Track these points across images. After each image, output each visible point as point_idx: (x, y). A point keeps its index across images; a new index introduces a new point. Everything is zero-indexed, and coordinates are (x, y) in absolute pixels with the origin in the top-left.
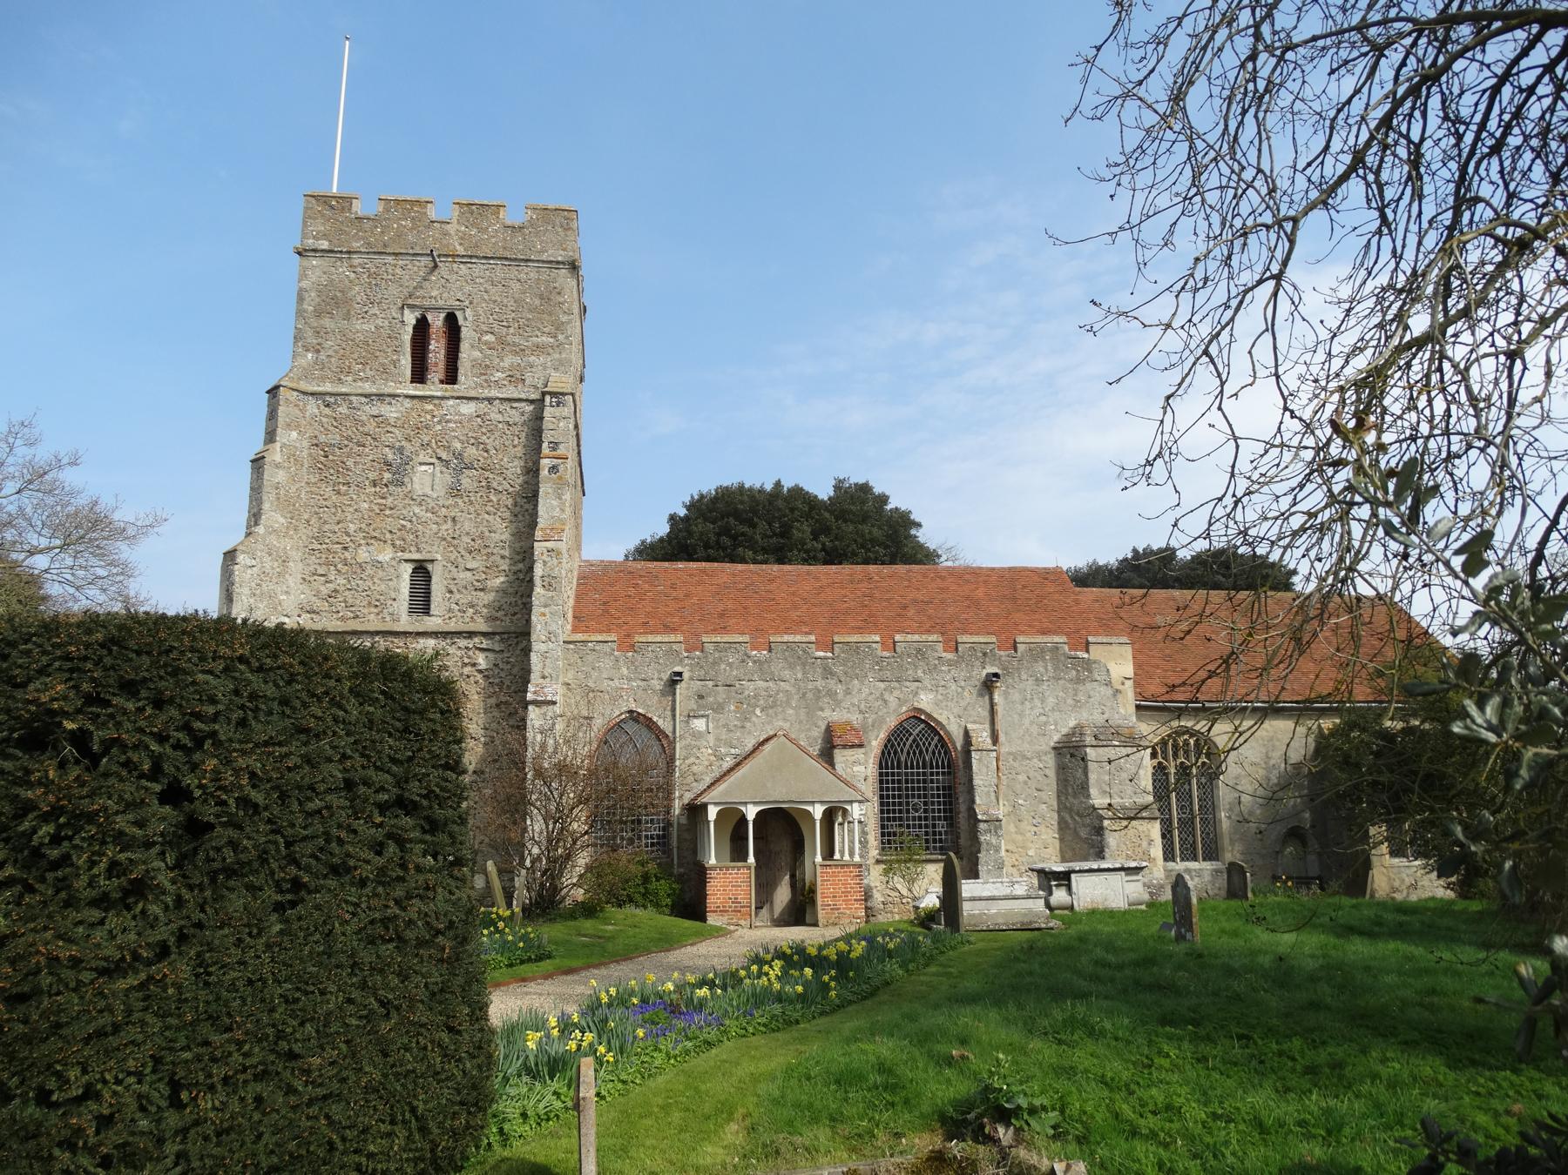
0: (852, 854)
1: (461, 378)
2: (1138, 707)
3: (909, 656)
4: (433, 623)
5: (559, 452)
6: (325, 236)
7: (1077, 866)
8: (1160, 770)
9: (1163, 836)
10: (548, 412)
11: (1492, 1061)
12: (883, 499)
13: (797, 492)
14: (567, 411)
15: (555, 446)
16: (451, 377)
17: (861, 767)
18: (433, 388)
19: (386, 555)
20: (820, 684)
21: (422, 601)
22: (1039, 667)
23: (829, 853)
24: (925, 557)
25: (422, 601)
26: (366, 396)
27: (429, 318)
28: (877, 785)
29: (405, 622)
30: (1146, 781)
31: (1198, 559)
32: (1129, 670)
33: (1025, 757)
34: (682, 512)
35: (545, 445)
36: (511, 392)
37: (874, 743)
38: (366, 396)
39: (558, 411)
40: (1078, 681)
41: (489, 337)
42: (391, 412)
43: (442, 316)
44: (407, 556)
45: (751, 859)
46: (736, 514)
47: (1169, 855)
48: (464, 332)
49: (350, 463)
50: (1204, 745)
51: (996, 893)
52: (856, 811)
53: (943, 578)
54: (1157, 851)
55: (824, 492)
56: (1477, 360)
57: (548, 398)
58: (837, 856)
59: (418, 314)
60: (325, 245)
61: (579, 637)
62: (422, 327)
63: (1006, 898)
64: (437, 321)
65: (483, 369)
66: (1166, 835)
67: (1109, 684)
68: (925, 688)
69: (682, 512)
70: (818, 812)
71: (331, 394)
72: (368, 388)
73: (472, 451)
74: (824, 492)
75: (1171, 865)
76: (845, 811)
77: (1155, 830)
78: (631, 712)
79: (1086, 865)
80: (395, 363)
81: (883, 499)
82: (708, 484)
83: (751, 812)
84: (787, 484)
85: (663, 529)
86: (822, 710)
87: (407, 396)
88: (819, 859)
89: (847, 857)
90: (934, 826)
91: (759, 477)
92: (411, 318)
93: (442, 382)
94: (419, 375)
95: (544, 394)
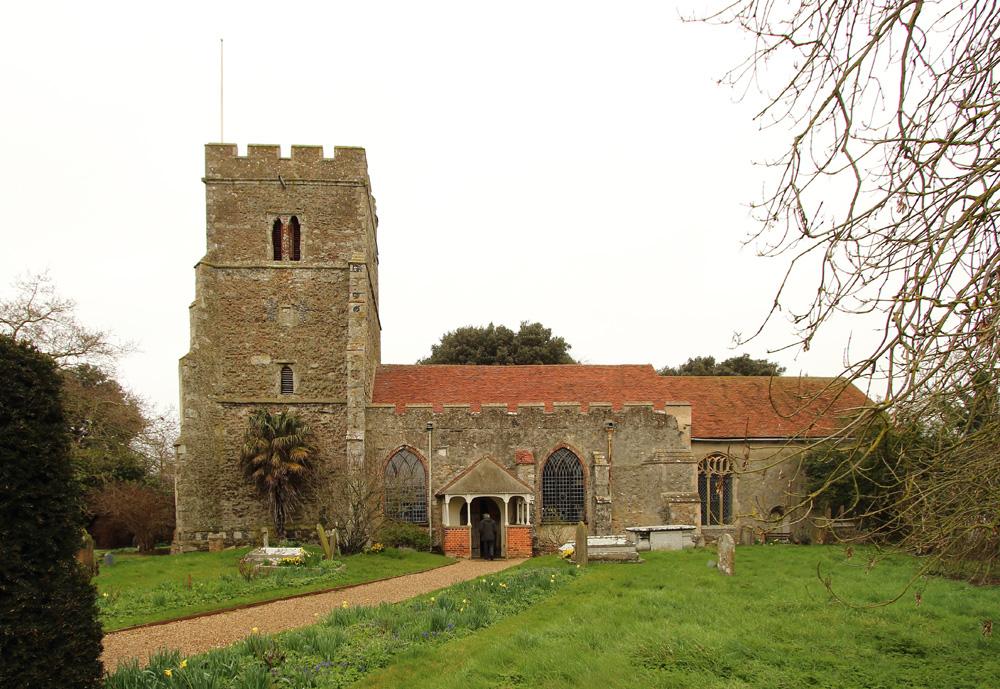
0: (525, 522)
1: (303, 257)
2: (693, 442)
3: (561, 414)
4: (293, 398)
5: (360, 299)
6: (219, 171)
7: (654, 528)
8: (702, 477)
9: (702, 512)
10: (352, 275)
11: (514, 573)
12: (548, 332)
13: (502, 330)
14: (363, 274)
15: (357, 295)
16: (296, 256)
17: (530, 475)
18: (286, 263)
19: (267, 360)
20: (511, 430)
21: (286, 387)
22: (636, 419)
23: (513, 520)
24: (569, 361)
25: (286, 387)
26: (249, 268)
27: (282, 221)
28: (541, 485)
29: (280, 398)
30: (695, 482)
31: (727, 364)
32: (689, 421)
33: (625, 470)
34: (439, 344)
35: (351, 295)
36: (330, 264)
37: (540, 463)
38: (249, 268)
39: (357, 275)
40: (659, 427)
41: (316, 231)
42: (264, 277)
43: (289, 218)
44: (279, 361)
45: (469, 524)
46: (468, 343)
47: (704, 522)
48: (303, 229)
49: (243, 308)
50: (727, 462)
51: (607, 543)
52: (528, 499)
53: (582, 371)
54: (698, 519)
55: (516, 329)
56: (964, 197)
57: (351, 266)
58: (518, 522)
59: (274, 218)
60: (219, 176)
61: (375, 405)
62: (278, 225)
63: (613, 546)
64: (286, 222)
65: (314, 250)
66: (703, 512)
67: (676, 428)
68: (570, 432)
69: (439, 344)
70: (506, 499)
71: (230, 268)
72: (249, 263)
73: (312, 300)
74: (516, 329)
75: (705, 527)
76: (522, 499)
77: (698, 508)
78: (405, 446)
79: (660, 527)
80: (264, 248)
81: (548, 332)
82: (452, 328)
83: (469, 499)
84: (496, 325)
85: (429, 354)
86: (511, 444)
87: (272, 268)
88: (507, 524)
89: (523, 523)
90: (573, 507)
91: (480, 322)
92: (271, 220)
93: (291, 259)
94: (278, 256)
95: (349, 264)
